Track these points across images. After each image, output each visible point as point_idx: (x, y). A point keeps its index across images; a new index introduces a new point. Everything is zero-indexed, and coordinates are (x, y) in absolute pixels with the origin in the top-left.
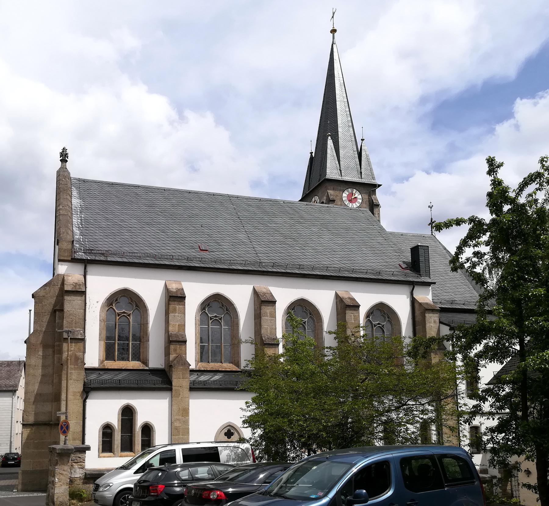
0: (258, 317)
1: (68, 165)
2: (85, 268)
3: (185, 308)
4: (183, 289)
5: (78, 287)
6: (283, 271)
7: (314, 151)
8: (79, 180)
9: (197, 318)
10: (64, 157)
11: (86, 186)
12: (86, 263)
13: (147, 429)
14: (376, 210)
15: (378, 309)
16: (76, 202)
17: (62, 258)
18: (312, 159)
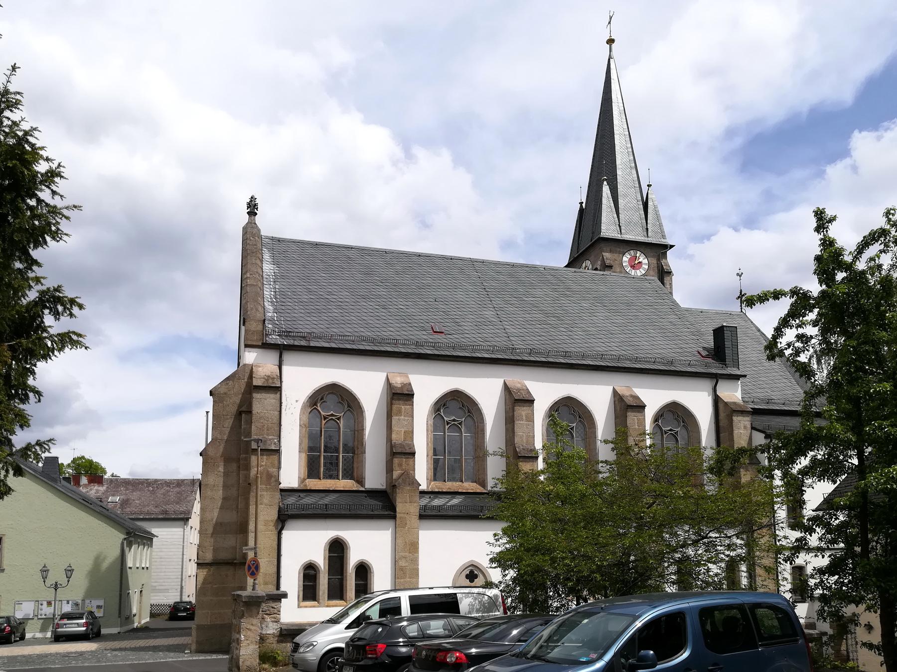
0: (510, 421)
5: (270, 381)
6: (544, 360)
8: (272, 239)
10: (252, 208)
11: (283, 248)
12: (281, 349)
13: (363, 570)
14: (666, 279)
16: (268, 268)
17: (249, 343)
18: (581, 211)
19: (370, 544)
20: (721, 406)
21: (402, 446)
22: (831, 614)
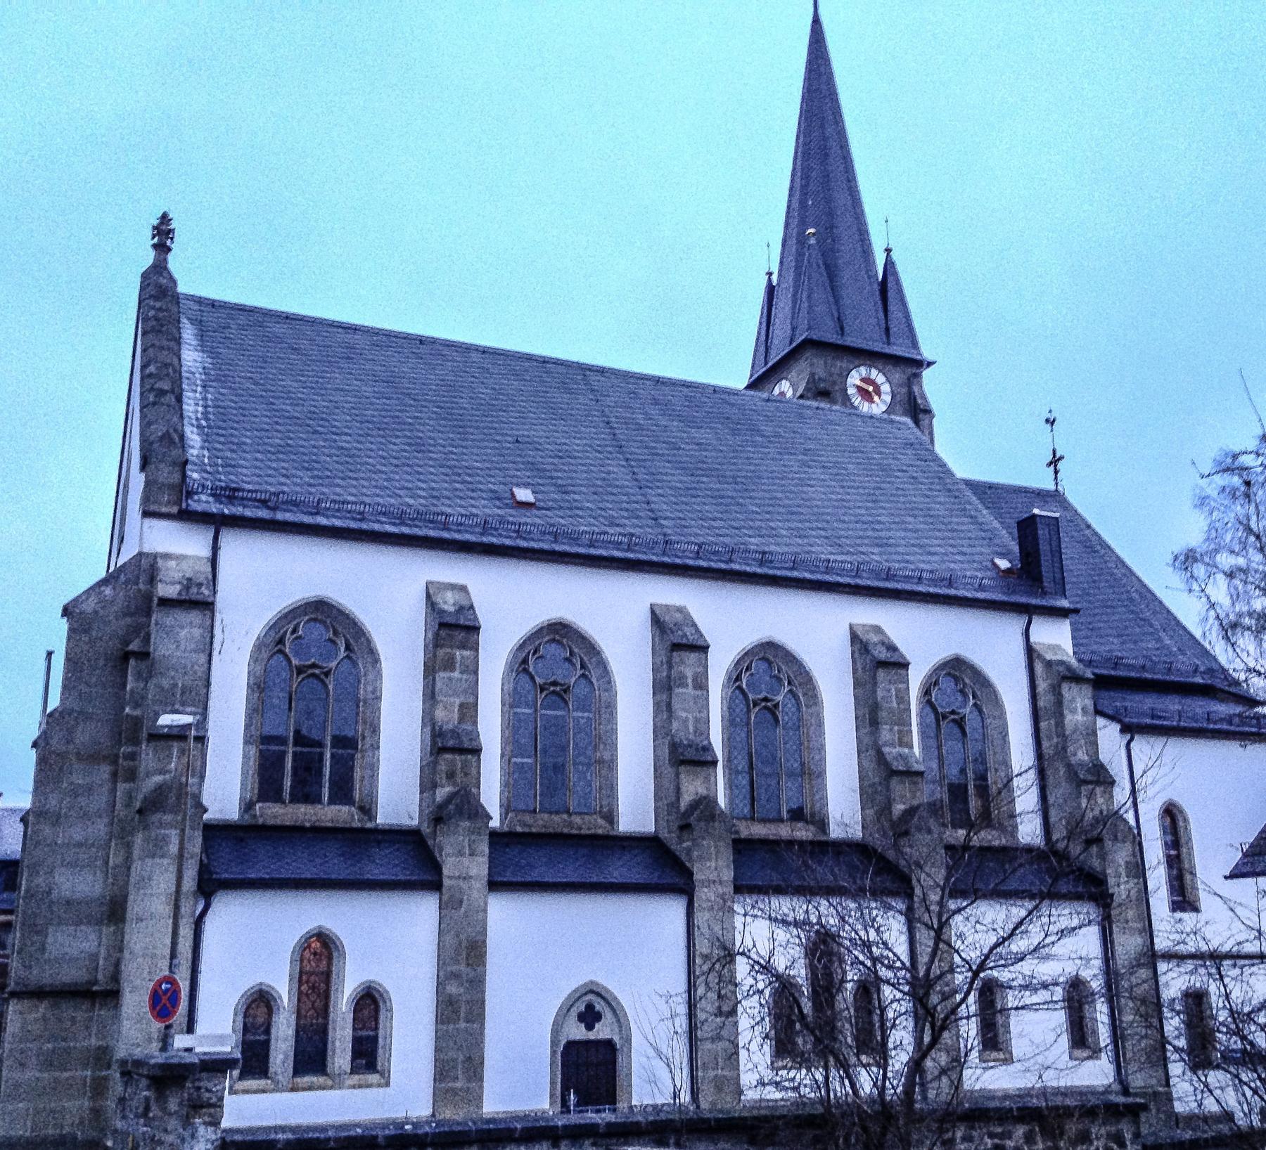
0: (664, 687)
1: (171, 257)
2: (216, 539)
4: (472, 607)
6: (723, 566)
7: (775, 270)
8: (200, 301)
9: (506, 687)
10: (163, 233)
11: (222, 319)
12: (218, 523)
13: (370, 1002)
14: (924, 420)
15: (949, 674)
16: (191, 357)
17: (153, 508)
18: (771, 291)
19: (389, 942)
20: (1039, 668)
21: (454, 733)
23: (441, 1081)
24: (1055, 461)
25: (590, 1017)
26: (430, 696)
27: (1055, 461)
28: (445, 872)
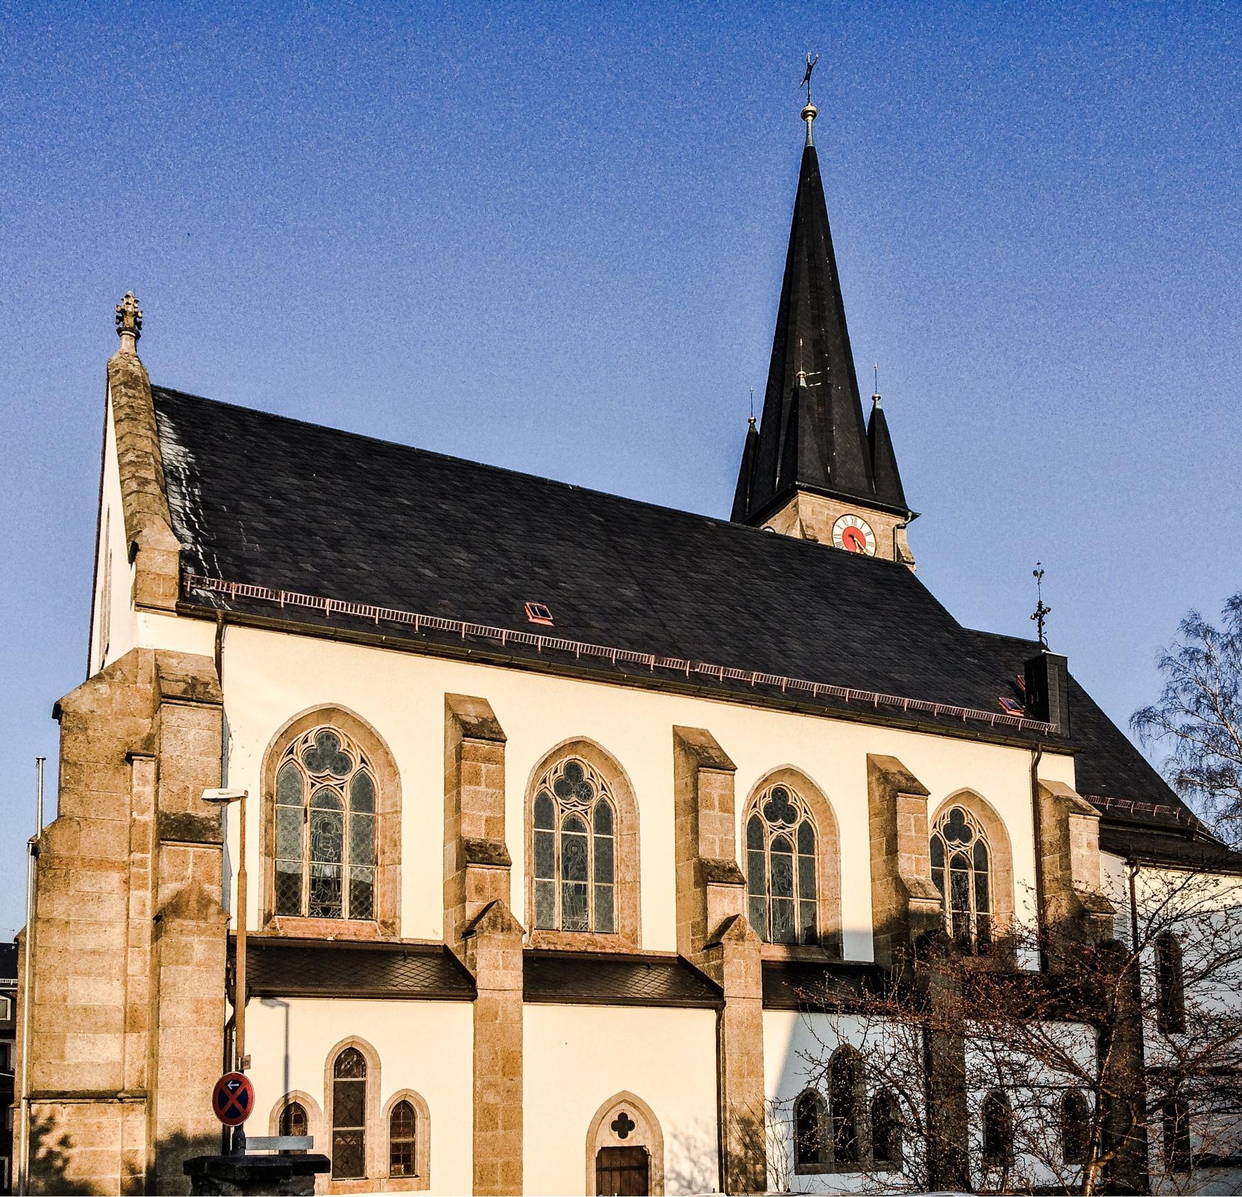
0: (690, 809)
3: (503, 770)
4: (495, 720)
5: (200, 689)
13: (404, 1116)
17: (147, 601)
20: (1046, 804)
22: (1168, 1121)
23: (480, 1184)
24: (1041, 613)
25: (623, 1125)
26: (455, 809)
27: (1041, 613)
28: (479, 984)
